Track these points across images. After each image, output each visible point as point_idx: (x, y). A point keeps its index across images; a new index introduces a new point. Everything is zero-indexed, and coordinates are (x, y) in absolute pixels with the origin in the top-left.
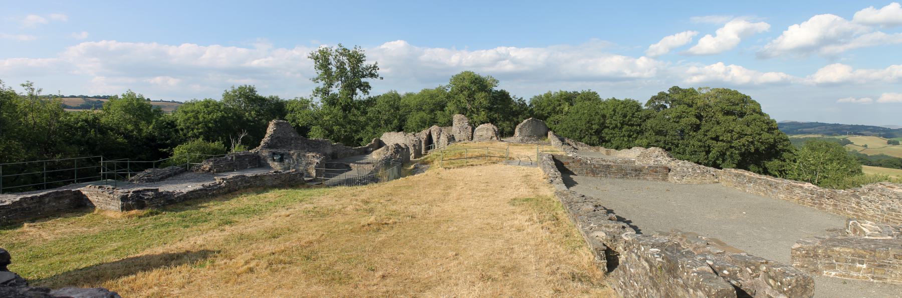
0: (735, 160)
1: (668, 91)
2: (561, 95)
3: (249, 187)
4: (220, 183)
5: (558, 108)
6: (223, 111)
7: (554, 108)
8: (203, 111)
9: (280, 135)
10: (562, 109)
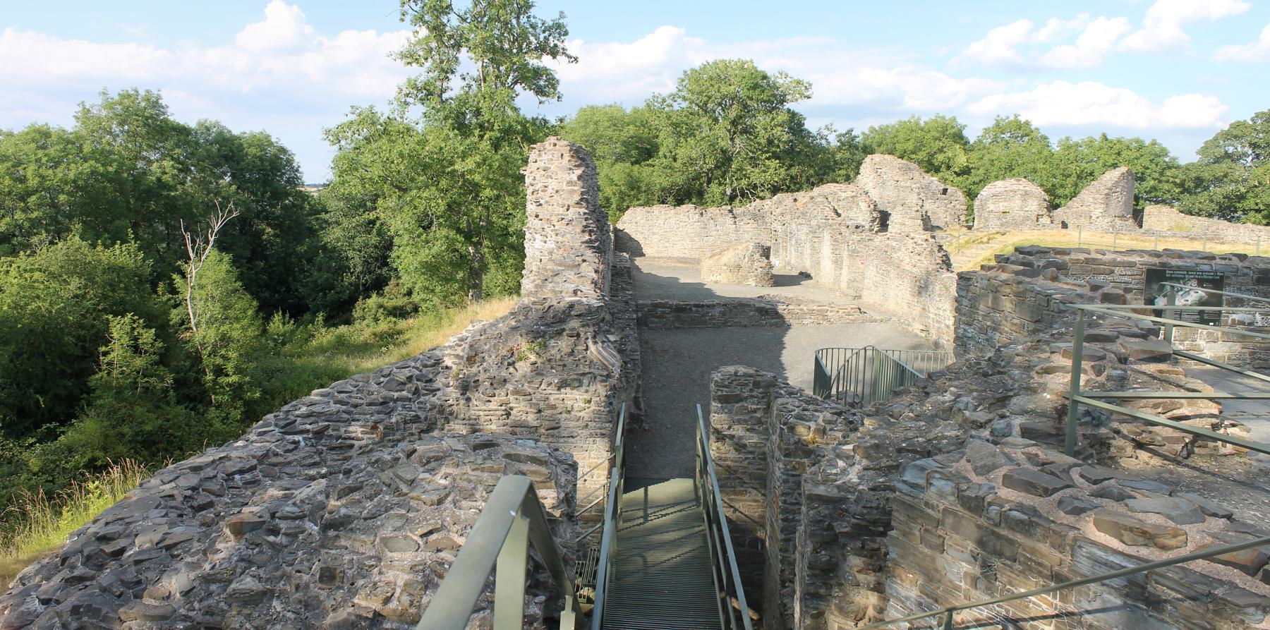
5: (940, 157)
6: (90, 158)
7: (932, 155)
8: (33, 158)
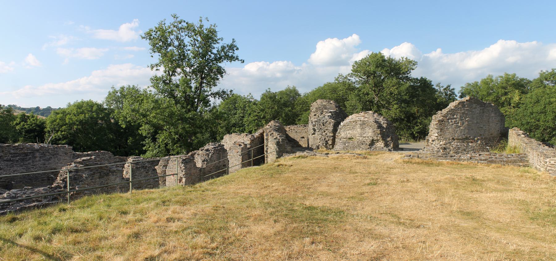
2: (508, 80)
5: (503, 98)
10: (510, 99)
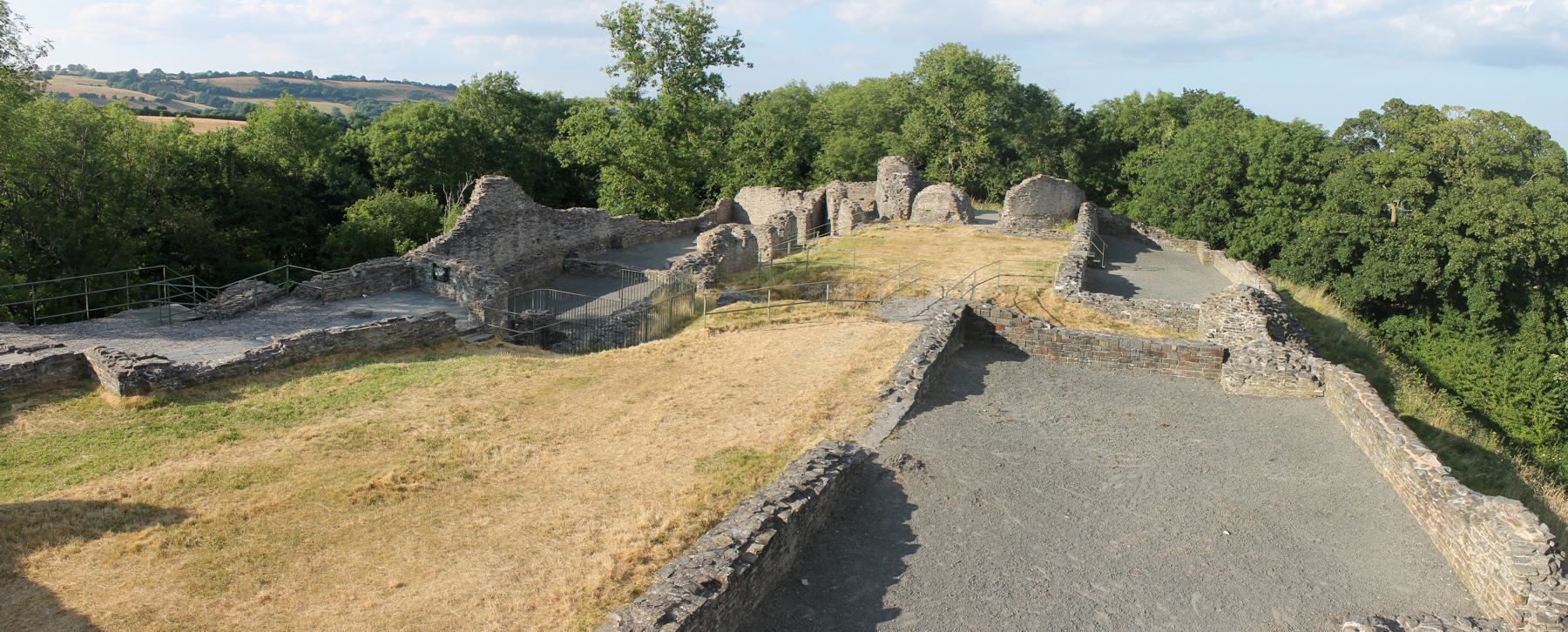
0: (1496, 283)
1: (1382, 108)
2: (1160, 103)
3: (332, 352)
4: (277, 349)
9: (493, 207)
